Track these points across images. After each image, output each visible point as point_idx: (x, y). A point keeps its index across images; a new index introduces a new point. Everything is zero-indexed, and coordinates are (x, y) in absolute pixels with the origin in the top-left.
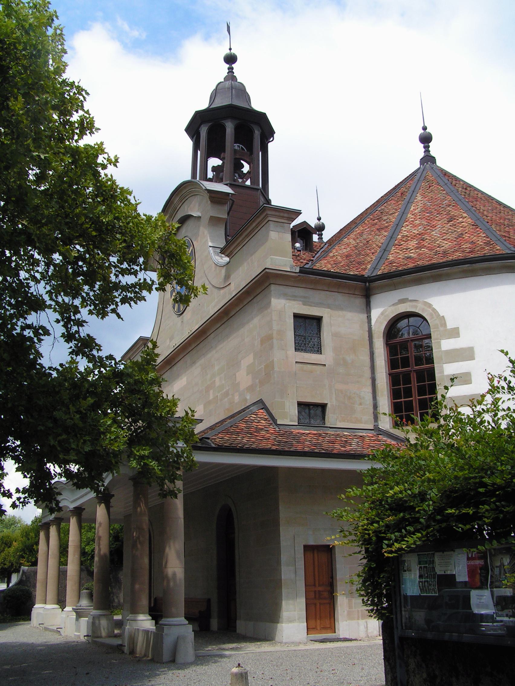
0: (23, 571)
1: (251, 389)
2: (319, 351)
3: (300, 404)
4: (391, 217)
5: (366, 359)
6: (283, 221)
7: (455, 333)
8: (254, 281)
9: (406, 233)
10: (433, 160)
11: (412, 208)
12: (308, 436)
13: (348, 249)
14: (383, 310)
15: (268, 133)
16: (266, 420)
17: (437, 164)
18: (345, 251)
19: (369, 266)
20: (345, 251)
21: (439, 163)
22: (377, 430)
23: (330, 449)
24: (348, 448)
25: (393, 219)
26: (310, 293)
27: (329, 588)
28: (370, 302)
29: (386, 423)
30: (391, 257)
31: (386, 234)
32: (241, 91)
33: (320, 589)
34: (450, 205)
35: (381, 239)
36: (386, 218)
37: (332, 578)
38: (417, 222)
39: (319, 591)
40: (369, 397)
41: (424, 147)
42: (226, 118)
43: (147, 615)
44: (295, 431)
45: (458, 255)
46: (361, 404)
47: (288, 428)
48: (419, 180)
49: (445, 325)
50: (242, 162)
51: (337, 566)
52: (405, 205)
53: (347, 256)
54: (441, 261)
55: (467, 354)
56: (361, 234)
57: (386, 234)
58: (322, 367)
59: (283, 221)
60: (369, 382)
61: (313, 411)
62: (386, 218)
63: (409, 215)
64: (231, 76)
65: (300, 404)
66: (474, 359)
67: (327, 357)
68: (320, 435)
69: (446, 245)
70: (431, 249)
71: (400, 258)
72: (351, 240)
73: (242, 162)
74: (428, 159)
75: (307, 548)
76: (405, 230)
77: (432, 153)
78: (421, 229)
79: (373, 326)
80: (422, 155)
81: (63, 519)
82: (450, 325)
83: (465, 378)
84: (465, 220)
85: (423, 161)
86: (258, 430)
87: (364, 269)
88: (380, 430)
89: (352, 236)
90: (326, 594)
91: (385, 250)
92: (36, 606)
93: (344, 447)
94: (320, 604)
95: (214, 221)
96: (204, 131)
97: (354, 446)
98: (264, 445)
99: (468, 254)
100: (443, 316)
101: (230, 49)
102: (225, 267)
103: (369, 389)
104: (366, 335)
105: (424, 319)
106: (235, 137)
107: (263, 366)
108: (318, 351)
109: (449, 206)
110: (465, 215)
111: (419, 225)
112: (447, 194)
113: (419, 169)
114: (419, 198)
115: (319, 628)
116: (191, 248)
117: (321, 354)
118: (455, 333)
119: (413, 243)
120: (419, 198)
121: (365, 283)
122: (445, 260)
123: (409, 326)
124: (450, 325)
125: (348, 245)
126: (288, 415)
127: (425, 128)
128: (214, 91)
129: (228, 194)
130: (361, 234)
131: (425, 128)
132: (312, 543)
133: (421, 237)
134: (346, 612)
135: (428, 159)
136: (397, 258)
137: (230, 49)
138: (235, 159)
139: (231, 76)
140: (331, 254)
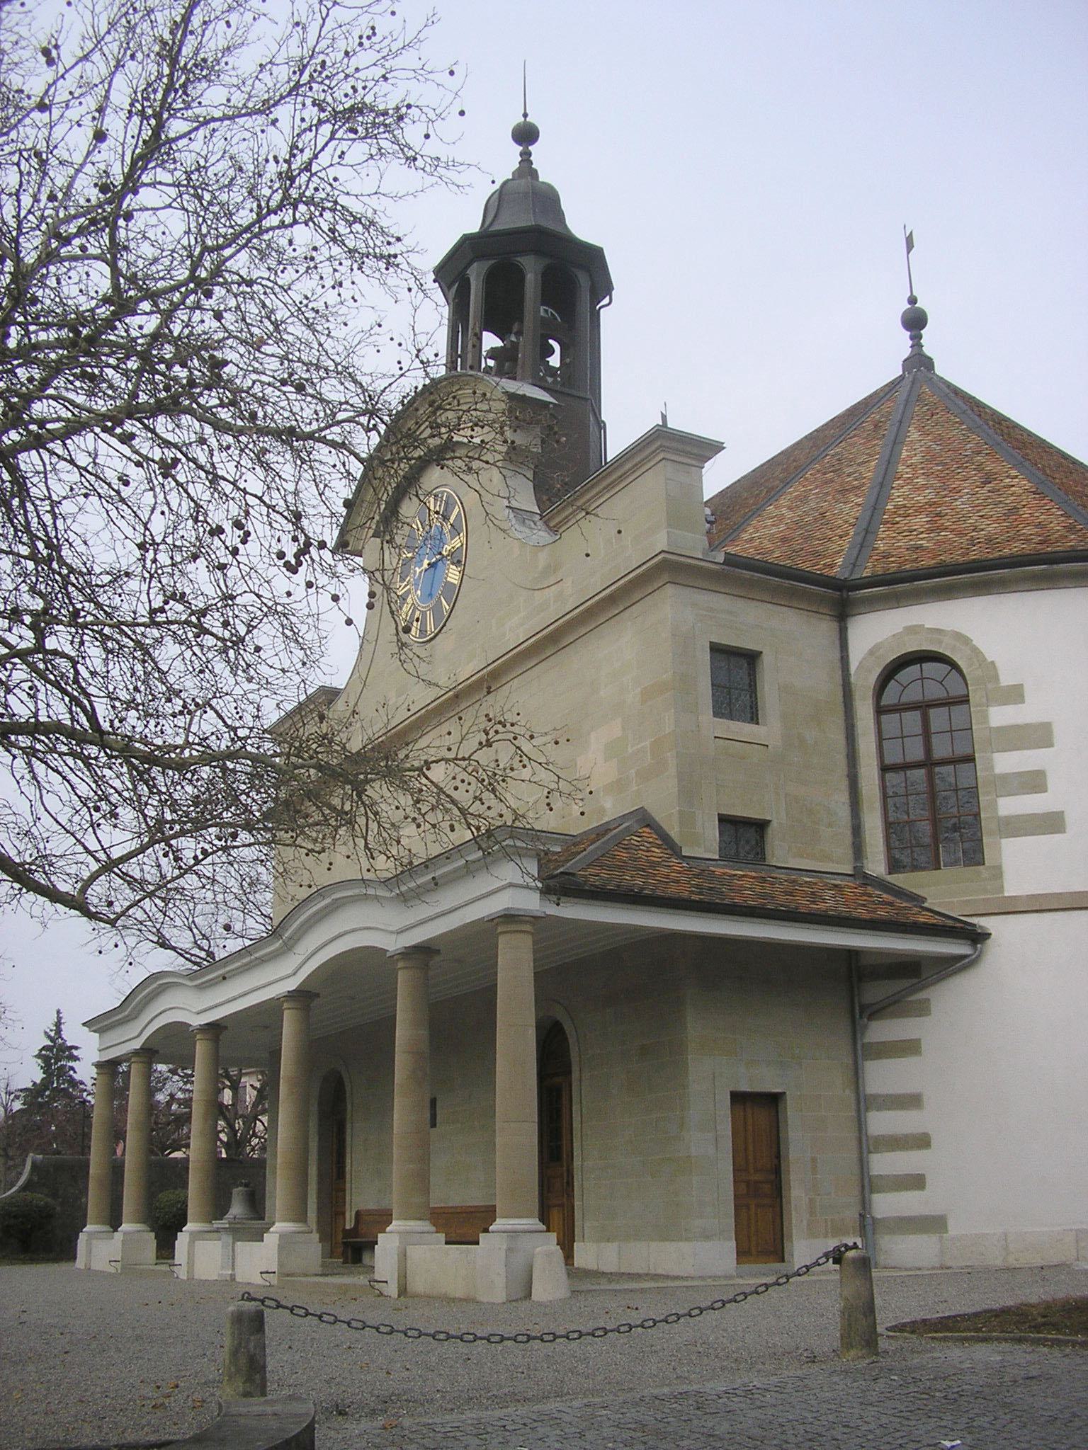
0: (33, 1163)
1: (618, 786)
2: (753, 717)
3: (723, 819)
4: (862, 469)
5: (839, 737)
6: (690, 461)
7: (1015, 695)
8: (631, 575)
9: (901, 501)
10: (928, 363)
11: (904, 454)
12: (744, 882)
13: (782, 527)
14: (878, 633)
15: (602, 286)
16: (659, 847)
17: (937, 371)
18: (774, 530)
19: (840, 561)
20: (774, 530)
21: (939, 370)
22: (860, 875)
23: (793, 905)
24: (821, 906)
25: (869, 472)
26: (741, 603)
27: (773, 1177)
28: (846, 629)
29: (876, 865)
30: (880, 545)
31: (859, 500)
32: (548, 200)
33: (757, 1177)
34: (980, 452)
35: (850, 510)
36: (848, 470)
37: (778, 1156)
38: (921, 481)
39: (756, 1182)
40: (844, 812)
41: (911, 338)
42: (523, 252)
43: (427, 1223)
44: (719, 871)
45: (1017, 548)
46: (830, 825)
47: (703, 865)
48: (907, 401)
49: (996, 678)
50: (551, 341)
51: (790, 1134)
52: (889, 448)
53: (784, 540)
54: (991, 556)
55: (1039, 735)
56: (804, 499)
57: (859, 500)
58: (439, 1104)
59: (690, 461)
60: (844, 784)
61: (745, 834)
62: (848, 470)
63: (901, 468)
64: (526, 168)
65: (723, 819)
66: (1051, 745)
67: (769, 730)
68: (764, 880)
69: (991, 528)
70: (960, 534)
71: (900, 547)
72: (784, 511)
73: (551, 341)
74: (919, 363)
75: (738, 1098)
76: (899, 495)
77: (927, 350)
78: (930, 494)
79: (853, 680)
80: (907, 352)
81: (157, 1052)
82: (1006, 680)
83: (1034, 782)
84: (1018, 484)
85: (908, 364)
86: (654, 865)
87: (832, 566)
88: (866, 876)
89: (784, 501)
90: (766, 1188)
91: (868, 533)
92: (88, 1228)
93: (813, 902)
94: (757, 1206)
95: (514, 454)
96: (476, 275)
97: (830, 904)
98: (673, 891)
99: (1040, 547)
100: (993, 663)
101: (525, 115)
102: (547, 549)
103: (843, 797)
104: (840, 694)
105: (954, 665)
106: (543, 290)
107: (648, 743)
108: (752, 719)
109: (979, 453)
110: (1014, 473)
111: (925, 486)
112: (969, 429)
113: (902, 378)
114: (914, 435)
115: (754, 1252)
116: (456, 510)
117: (757, 723)
118: (1015, 695)
119: (920, 521)
120: (914, 435)
121: (840, 590)
122: (997, 555)
123: (922, 679)
124: (1006, 680)
125: (781, 518)
126: (705, 842)
127: (912, 300)
128: (496, 196)
129: (546, 404)
130: (804, 499)
131: (912, 300)
132: (745, 1087)
133: (935, 512)
134: (805, 1222)
135: (919, 363)
136: (893, 547)
137: (525, 115)
138: (542, 335)
139: (526, 168)
140: (746, 536)
